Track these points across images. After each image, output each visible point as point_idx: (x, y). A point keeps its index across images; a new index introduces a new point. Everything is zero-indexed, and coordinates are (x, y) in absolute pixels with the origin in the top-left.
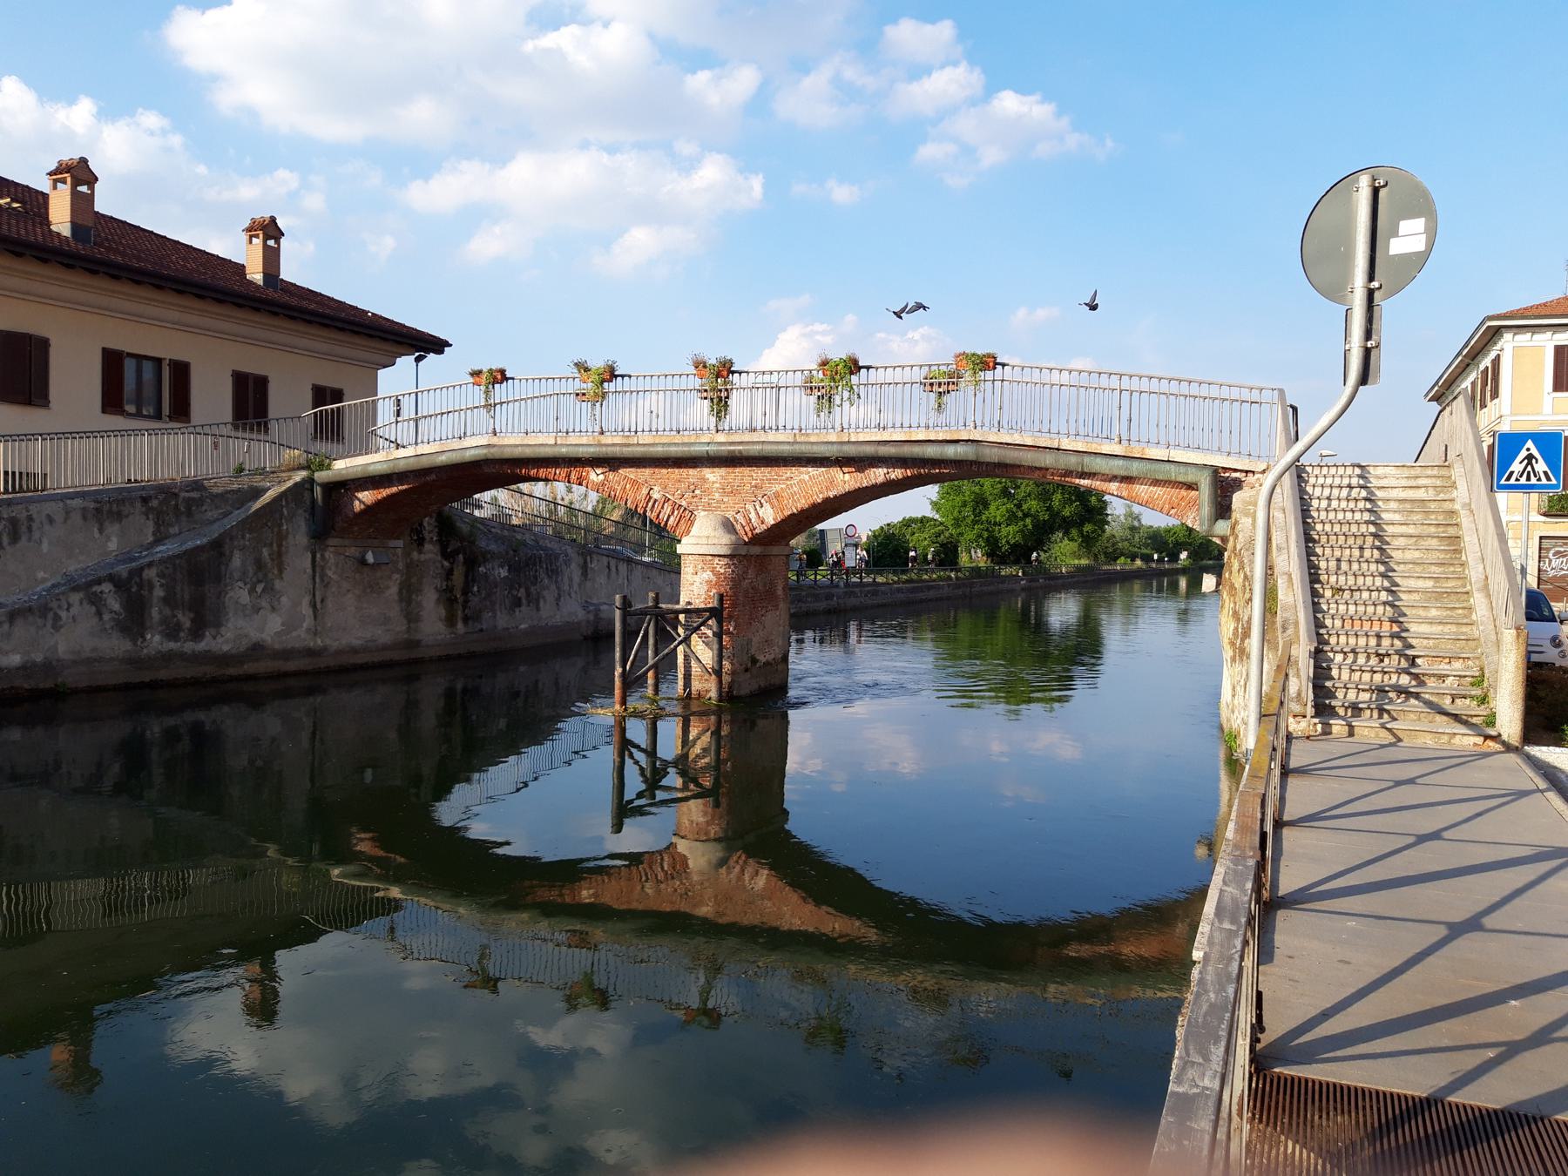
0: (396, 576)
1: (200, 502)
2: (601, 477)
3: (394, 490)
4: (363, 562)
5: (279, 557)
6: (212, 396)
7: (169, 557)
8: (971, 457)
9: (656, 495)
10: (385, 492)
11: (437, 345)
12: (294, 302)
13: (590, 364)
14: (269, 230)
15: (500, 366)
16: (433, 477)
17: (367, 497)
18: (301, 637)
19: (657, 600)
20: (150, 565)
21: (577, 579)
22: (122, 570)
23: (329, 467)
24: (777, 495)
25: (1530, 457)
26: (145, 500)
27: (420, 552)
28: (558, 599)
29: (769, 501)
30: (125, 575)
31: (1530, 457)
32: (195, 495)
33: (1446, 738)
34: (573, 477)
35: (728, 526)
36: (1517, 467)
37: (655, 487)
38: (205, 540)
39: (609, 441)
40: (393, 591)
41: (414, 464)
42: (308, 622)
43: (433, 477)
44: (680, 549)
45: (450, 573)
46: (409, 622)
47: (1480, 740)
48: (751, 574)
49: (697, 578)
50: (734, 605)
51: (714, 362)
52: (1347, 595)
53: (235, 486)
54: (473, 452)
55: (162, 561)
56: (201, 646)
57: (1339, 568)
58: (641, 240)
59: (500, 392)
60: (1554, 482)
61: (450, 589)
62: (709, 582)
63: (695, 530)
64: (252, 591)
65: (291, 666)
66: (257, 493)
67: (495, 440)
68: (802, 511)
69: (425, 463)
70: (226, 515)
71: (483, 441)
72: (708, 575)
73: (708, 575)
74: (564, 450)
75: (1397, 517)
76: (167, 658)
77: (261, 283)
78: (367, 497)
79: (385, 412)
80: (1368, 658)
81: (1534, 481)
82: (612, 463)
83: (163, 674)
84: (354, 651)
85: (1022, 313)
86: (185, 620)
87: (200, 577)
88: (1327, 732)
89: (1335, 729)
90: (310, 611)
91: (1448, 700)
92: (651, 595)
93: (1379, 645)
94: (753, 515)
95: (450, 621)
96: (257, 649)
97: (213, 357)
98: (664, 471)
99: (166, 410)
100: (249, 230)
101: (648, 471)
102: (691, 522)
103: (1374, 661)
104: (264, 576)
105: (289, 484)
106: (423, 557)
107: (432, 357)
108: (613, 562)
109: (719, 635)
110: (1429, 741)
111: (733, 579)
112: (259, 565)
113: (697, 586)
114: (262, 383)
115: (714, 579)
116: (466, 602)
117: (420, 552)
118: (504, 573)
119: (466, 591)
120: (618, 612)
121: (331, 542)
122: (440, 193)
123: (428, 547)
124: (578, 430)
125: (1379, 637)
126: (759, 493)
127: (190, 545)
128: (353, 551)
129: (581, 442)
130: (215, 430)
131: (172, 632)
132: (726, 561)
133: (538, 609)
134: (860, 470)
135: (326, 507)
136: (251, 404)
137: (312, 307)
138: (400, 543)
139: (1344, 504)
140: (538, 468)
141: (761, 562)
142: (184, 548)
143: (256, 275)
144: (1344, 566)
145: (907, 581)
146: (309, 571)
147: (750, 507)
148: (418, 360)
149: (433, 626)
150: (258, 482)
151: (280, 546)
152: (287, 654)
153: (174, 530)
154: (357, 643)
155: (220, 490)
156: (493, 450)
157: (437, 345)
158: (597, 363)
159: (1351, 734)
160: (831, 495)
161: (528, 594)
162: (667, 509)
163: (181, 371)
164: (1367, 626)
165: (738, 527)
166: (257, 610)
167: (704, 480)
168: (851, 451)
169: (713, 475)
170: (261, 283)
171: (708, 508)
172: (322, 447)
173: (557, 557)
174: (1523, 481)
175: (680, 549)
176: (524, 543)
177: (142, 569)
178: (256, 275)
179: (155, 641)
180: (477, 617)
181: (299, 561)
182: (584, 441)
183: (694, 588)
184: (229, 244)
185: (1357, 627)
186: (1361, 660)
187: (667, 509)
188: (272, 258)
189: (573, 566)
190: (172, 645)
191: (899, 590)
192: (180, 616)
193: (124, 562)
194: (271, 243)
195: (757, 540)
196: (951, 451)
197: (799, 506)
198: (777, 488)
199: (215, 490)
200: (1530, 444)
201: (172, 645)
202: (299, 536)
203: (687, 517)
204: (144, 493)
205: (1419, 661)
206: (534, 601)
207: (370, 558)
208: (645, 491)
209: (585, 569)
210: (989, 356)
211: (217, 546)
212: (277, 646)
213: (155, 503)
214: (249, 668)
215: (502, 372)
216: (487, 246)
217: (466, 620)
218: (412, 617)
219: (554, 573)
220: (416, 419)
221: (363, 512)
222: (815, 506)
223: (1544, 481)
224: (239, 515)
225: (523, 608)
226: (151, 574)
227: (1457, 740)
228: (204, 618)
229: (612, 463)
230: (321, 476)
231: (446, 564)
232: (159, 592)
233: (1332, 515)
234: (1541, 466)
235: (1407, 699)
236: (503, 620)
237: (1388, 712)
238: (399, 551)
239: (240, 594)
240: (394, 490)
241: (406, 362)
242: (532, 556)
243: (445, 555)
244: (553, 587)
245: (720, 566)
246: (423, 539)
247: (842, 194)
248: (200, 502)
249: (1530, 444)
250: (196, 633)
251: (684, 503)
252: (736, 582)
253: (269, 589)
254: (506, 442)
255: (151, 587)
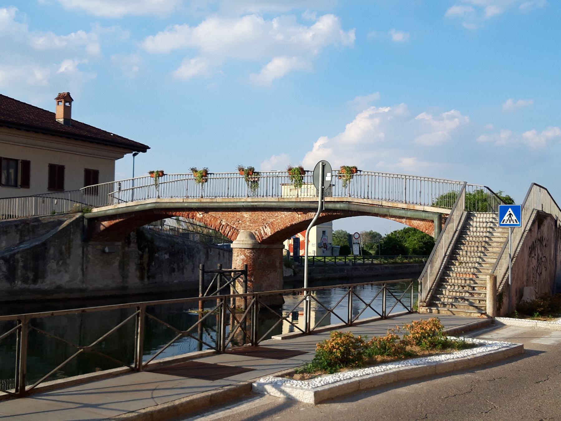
0: (118, 258)
1: (37, 227)
2: (201, 216)
3: (117, 221)
4: (104, 252)
5: (69, 249)
6: (39, 176)
7: (25, 250)
8: (347, 209)
9: (223, 223)
10: (113, 222)
11: (143, 148)
12: (77, 131)
13: (197, 169)
14: (66, 98)
15: (162, 170)
16: (133, 215)
17: (106, 224)
18: (77, 284)
19: (221, 267)
20: (18, 253)
21: (203, 260)
22: (7, 254)
23: (90, 212)
24: (272, 223)
25: (510, 214)
26: (16, 226)
27: (129, 247)
28: (193, 269)
29: (269, 226)
30: (8, 257)
31: (510, 214)
32: (36, 224)
33: (469, 314)
34: (190, 216)
35: (252, 236)
36: (506, 218)
37: (224, 220)
38: (40, 242)
39: (205, 201)
40: (117, 264)
41: (125, 210)
42: (80, 277)
43: (133, 215)
44: (232, 246)
45: (141, 257)
46: (123, 278)
47: (479, 315)
48: (262, 256)
49: (238, 258)
50: (253, 270)
51: (246, 168)
52: (464, 265)
53: (52, 220)
54: (149, 205)
55: (23, 251)
56: (37, 286)
57: (467, 254)
58: (278, 66)
59: (161, 180)
60: (518, 223)
61: (141, 264)
62: (243, 259)
63: (238, 238)
64: (57, 264)
65: (72, 296)
66: (61, 222)
67: (159, 200)
68: (282, 230)
69: (130, 210)
70: (48, 232)
71: (154, 200)
72: (242, 257)
73: (242, 257)
74: (186, 205)
75: (499, 235)
76: (23, 291)
77: (63, 123)
78: (106, 224)
79: (116, 187)
80: (459, 287)
81: (512, 223)
82: (206, 210)
83: (21, 298)
84: (99, 290)
85: (509, 102)
86: (31, 275)
87: (38, 256)
88: (431, 312)
89: (434, 311)
90: (81, 273)
91: (478, 302)
92: (219, 265)
93: (465, 283)
94: (262, 232)
95: (142, 278)
96: (59, 288)
97: (40, 157)
98: (227, 213)
99: (19, 183)
100: (57, 99)
101: (220, 213)
102: (237, 234)
103: (461, 288)
104: (63, 257)
105: (74, 219)
106: (130, 249)
107: (141, 154)
108: (221, 252)
109: (246, 282)
110: (463, 315)
111: (253, 259)
112: (61, 253)
113: (238, 262)
114: (61, 169)
115: (246, 259)
116: (149, 269)
117: (129, 247)
118: (167, 256)
119: (149, 265)
120: (201, 271)
121: (91, 243)
122: (162, 43)
123: (132, 245)
124: (194, 194)
125: (465, 280)
126: (265, 222)
127: (34, 244)
128: (99, 247)
129: (193, 201)
130: (44, 195)
131: (25, 280)
132: (250, 251)
133: (183, 273)
134: (305, 213)
135: (89, 228)
136: (56, 180)
137: (85, 133)
138: (120, 243)
139: (482, 229)
140: (176, 212)
141: (268, 252)
142: (31, 246)
143: (60, 118)
144: (469, 254)
145: (393, 263)
146: (81, 255)
147: (261, 228)
148: (134, 155)
149: (133, 279)
150: (62, 218)
151: (69, 244)
152: (71, 291)
153: (27, 238)
154: (100, 286)
155: (46, 222)
156: (157, 205)
157: (143, 148)
158: (200, 168)
159: (439, 313)
160: (293, 223)
161: (178, 266)
162: (228, 229)
163: (26, 165)
164: (464, 276)
165: (256, 236)
166: (59, 271)
167: (243, 217)
168: (300, 205)
169: (246, 215)
170: (63, 123)
171: (244, 228)
172: (89, 199)
173: (193, 249)
174: (508, 223)
175: (232, 246)
176: (178, 243)
177: (14, 254)
178: (60, 118)
179: (19, 284)
180: (154, 277)
181: (77, 251)
182: (195, 200)
183: (237, 262)
184: (46, 102)
185: (461, 277)
186: (456, 288)
187: (228, 229)
188: (67, 111)
189: (201, 253)
190: (25, 286)
191: (386, 268)
192: (29, 274)
193: (8, 251)
194: (67, 104)
195: (264, 242)
196: (338, 206)
197: (281, 228)
198: (272, 220)
199: (44, 222)
200: (510, 210)
201: (25, 286)
202: (77, 240)
203: (236, 232)
204: (16, 223)
205: (476, 288)
206: (182, 270)
207: (107, 250)
208: (219, 221)
209: (207, 255)
210: (354, 167)
211: (44, 244)
212: (67, 287)
213: (20, 227)
214: (55, 296)
215: (162, 172)
216: (189, 70)
217: (149, 278)
218: (124, 276)
219: (191, 257)
220: (131, 185)
221: (104, 230)
222: (287, 228)
223: (515, 223)
224: (53, 232)
225: (176, 273)
226: (18, 256)
227: (472, 315)
228: (39, 275)
229: (206, 210)
230: (87, 215)
231: (140, 252)
232: (21, 264)
233: (478, 234)
234: (514, 218)
235: (464, 301)
236: (165, 278)
237: (454, 305)
238: (120, 247)
239: (52, 265)
240: (117, 221)
241: (128, 156)
242: (181, 248)
243: (140, 248)
244: (191, 263)
245: (247, 252)
246: (130, 241)
247: (398, 37)
248: (37, 227)
249: (510, 210)
250: (35, 281)
251: (235, 226)
252: (255, 260)
253: (65, 263)
254: (163, 201)
255: (18, 262)
